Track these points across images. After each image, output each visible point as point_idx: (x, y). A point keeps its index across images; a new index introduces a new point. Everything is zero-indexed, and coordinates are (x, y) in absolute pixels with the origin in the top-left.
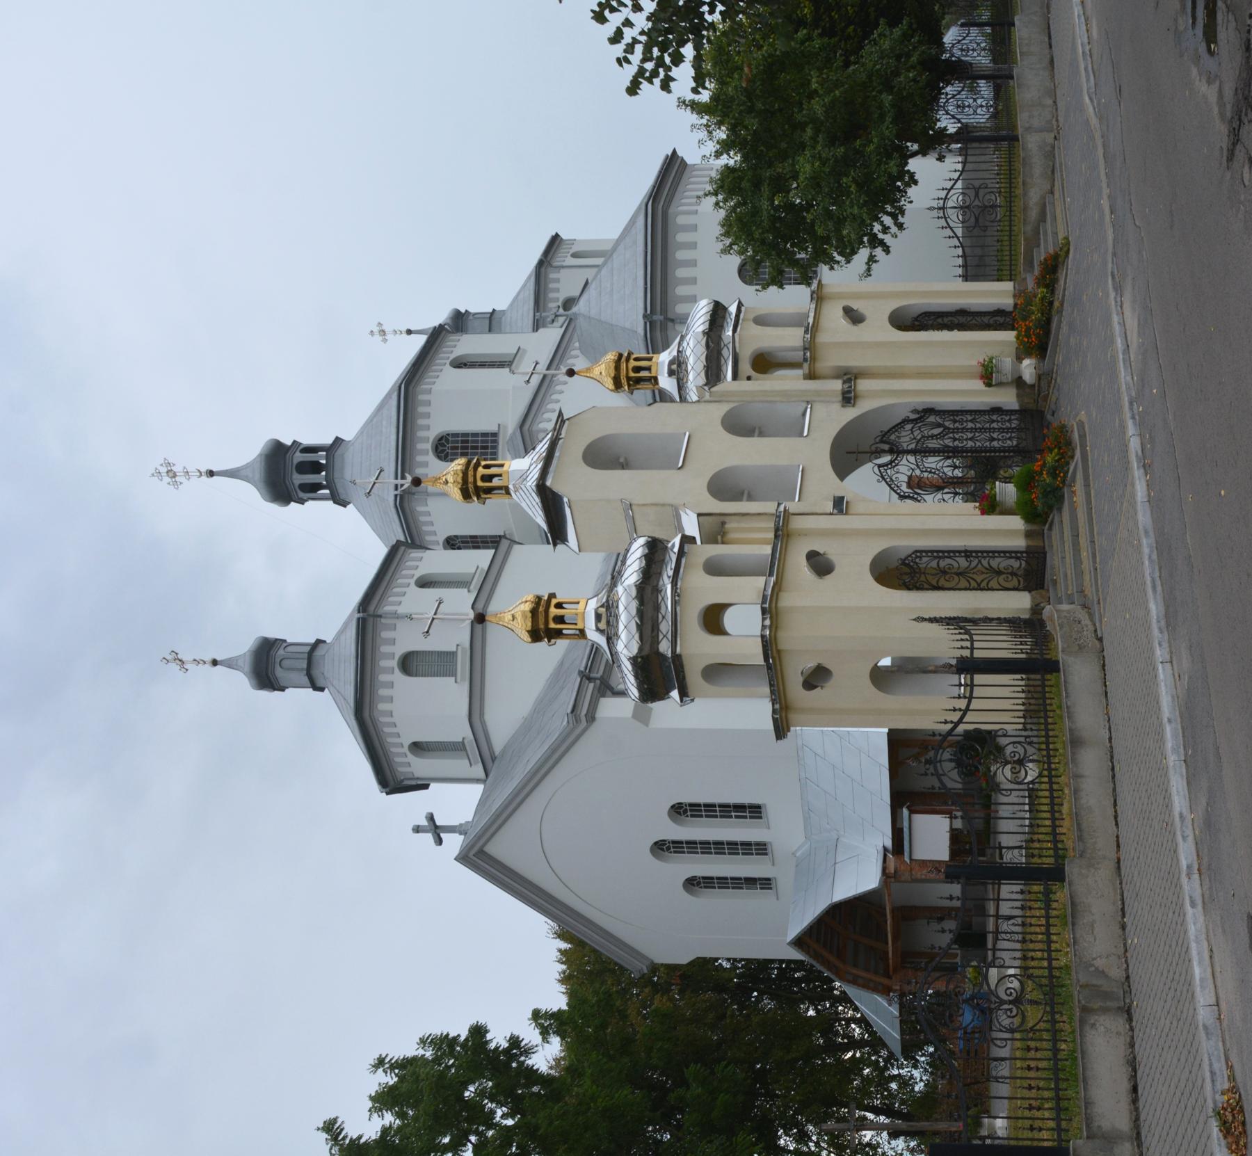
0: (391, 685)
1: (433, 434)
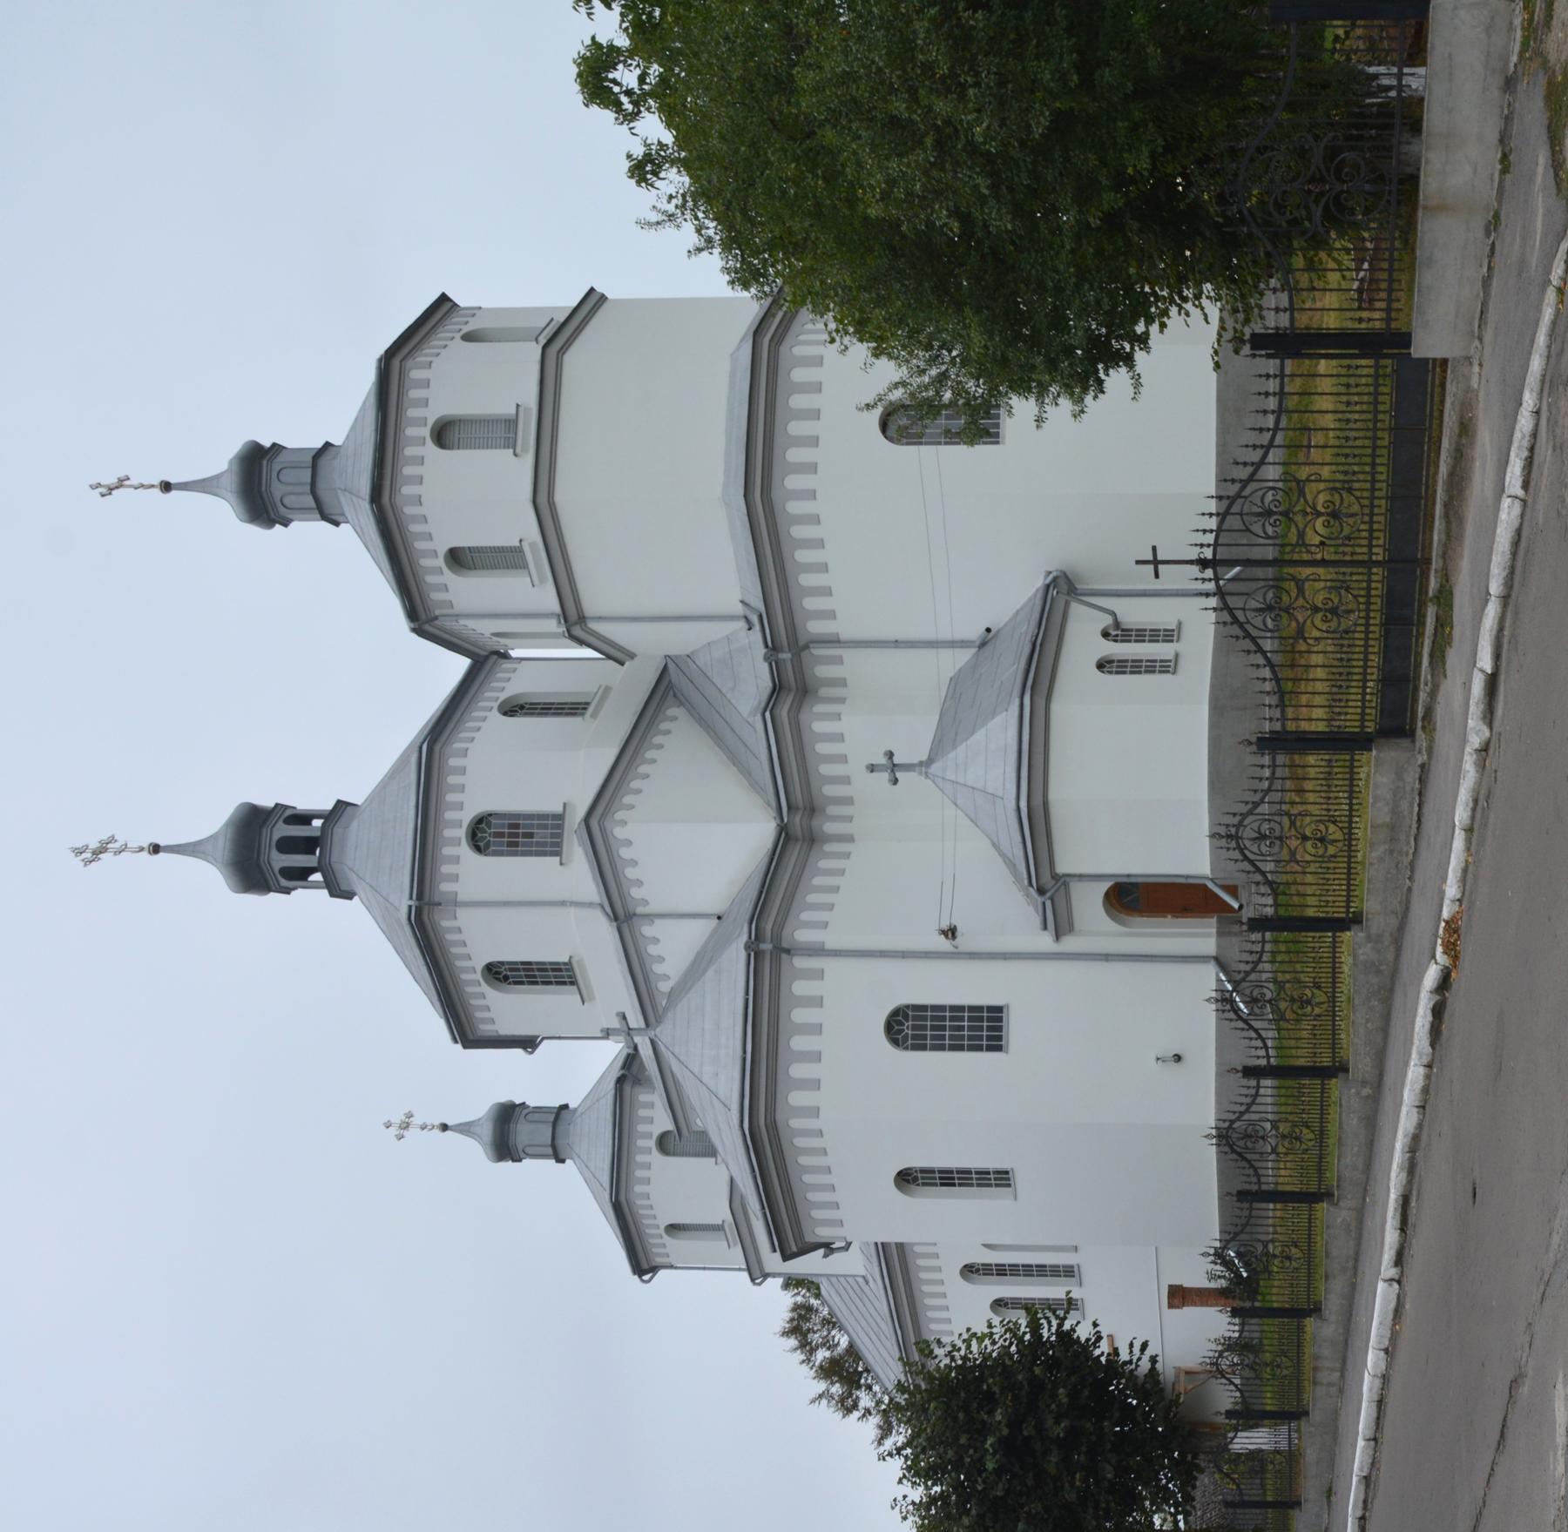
0: (421, 461)
1: (467, 816)
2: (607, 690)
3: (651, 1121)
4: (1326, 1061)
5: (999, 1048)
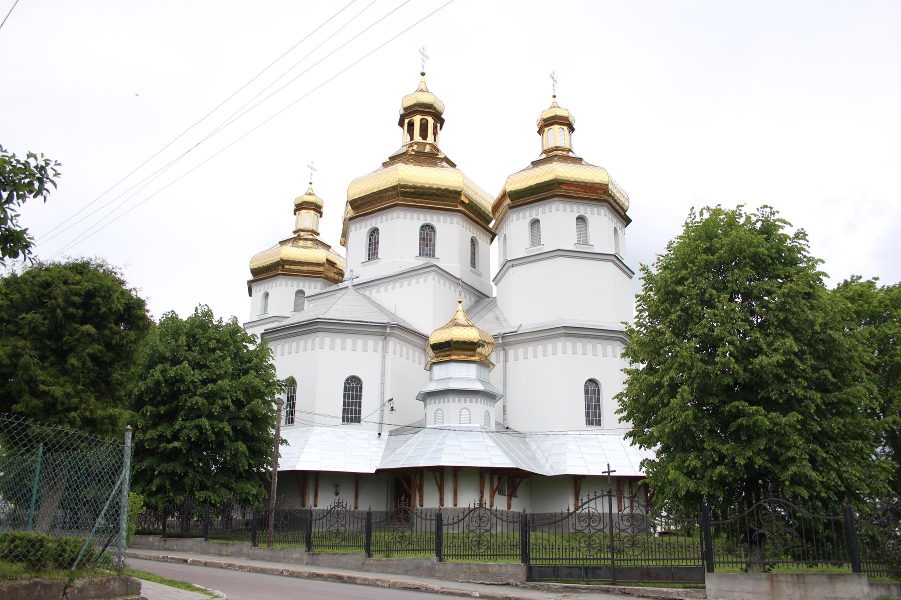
1: (435, 223)
2: (480, 276)
3: (310, 288)
4: (445, 551)
5: (343, 421)
